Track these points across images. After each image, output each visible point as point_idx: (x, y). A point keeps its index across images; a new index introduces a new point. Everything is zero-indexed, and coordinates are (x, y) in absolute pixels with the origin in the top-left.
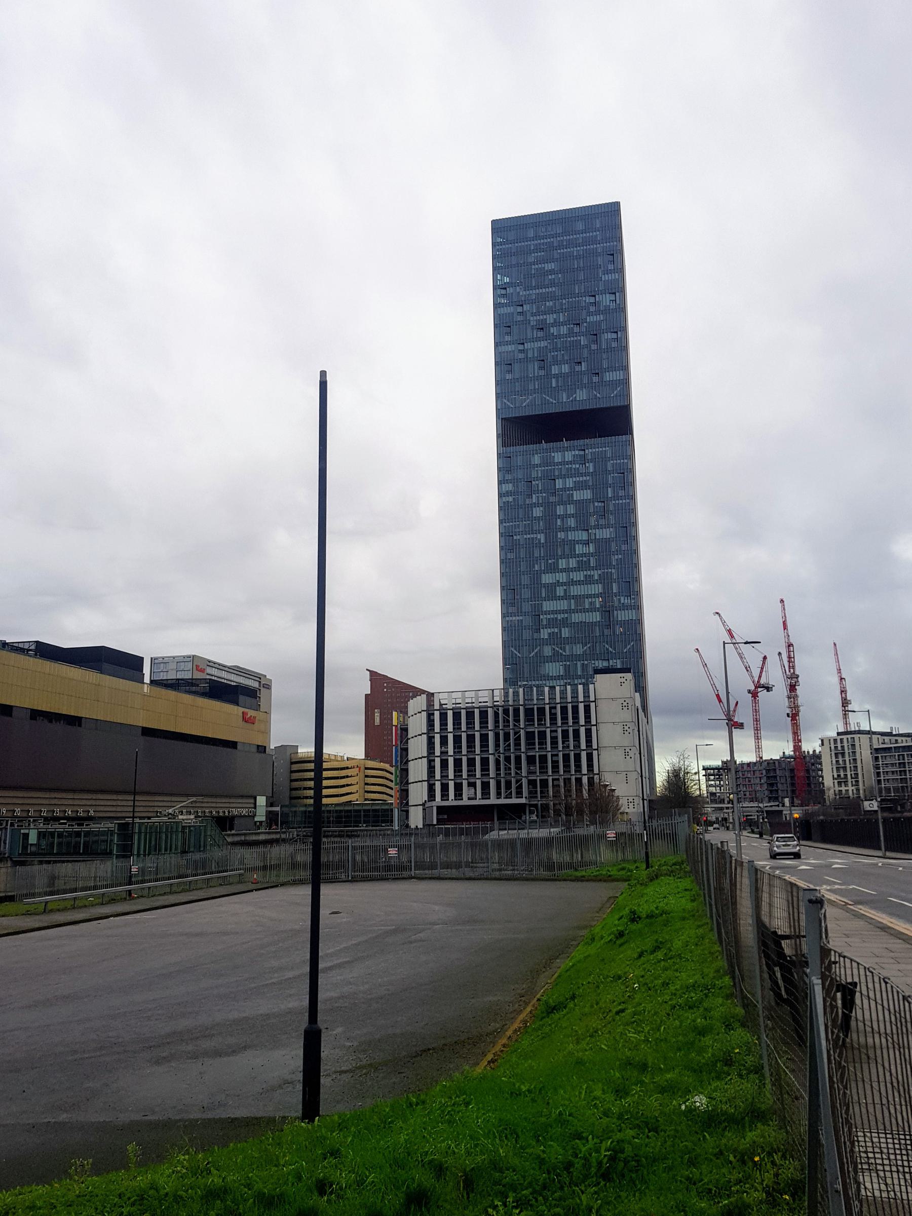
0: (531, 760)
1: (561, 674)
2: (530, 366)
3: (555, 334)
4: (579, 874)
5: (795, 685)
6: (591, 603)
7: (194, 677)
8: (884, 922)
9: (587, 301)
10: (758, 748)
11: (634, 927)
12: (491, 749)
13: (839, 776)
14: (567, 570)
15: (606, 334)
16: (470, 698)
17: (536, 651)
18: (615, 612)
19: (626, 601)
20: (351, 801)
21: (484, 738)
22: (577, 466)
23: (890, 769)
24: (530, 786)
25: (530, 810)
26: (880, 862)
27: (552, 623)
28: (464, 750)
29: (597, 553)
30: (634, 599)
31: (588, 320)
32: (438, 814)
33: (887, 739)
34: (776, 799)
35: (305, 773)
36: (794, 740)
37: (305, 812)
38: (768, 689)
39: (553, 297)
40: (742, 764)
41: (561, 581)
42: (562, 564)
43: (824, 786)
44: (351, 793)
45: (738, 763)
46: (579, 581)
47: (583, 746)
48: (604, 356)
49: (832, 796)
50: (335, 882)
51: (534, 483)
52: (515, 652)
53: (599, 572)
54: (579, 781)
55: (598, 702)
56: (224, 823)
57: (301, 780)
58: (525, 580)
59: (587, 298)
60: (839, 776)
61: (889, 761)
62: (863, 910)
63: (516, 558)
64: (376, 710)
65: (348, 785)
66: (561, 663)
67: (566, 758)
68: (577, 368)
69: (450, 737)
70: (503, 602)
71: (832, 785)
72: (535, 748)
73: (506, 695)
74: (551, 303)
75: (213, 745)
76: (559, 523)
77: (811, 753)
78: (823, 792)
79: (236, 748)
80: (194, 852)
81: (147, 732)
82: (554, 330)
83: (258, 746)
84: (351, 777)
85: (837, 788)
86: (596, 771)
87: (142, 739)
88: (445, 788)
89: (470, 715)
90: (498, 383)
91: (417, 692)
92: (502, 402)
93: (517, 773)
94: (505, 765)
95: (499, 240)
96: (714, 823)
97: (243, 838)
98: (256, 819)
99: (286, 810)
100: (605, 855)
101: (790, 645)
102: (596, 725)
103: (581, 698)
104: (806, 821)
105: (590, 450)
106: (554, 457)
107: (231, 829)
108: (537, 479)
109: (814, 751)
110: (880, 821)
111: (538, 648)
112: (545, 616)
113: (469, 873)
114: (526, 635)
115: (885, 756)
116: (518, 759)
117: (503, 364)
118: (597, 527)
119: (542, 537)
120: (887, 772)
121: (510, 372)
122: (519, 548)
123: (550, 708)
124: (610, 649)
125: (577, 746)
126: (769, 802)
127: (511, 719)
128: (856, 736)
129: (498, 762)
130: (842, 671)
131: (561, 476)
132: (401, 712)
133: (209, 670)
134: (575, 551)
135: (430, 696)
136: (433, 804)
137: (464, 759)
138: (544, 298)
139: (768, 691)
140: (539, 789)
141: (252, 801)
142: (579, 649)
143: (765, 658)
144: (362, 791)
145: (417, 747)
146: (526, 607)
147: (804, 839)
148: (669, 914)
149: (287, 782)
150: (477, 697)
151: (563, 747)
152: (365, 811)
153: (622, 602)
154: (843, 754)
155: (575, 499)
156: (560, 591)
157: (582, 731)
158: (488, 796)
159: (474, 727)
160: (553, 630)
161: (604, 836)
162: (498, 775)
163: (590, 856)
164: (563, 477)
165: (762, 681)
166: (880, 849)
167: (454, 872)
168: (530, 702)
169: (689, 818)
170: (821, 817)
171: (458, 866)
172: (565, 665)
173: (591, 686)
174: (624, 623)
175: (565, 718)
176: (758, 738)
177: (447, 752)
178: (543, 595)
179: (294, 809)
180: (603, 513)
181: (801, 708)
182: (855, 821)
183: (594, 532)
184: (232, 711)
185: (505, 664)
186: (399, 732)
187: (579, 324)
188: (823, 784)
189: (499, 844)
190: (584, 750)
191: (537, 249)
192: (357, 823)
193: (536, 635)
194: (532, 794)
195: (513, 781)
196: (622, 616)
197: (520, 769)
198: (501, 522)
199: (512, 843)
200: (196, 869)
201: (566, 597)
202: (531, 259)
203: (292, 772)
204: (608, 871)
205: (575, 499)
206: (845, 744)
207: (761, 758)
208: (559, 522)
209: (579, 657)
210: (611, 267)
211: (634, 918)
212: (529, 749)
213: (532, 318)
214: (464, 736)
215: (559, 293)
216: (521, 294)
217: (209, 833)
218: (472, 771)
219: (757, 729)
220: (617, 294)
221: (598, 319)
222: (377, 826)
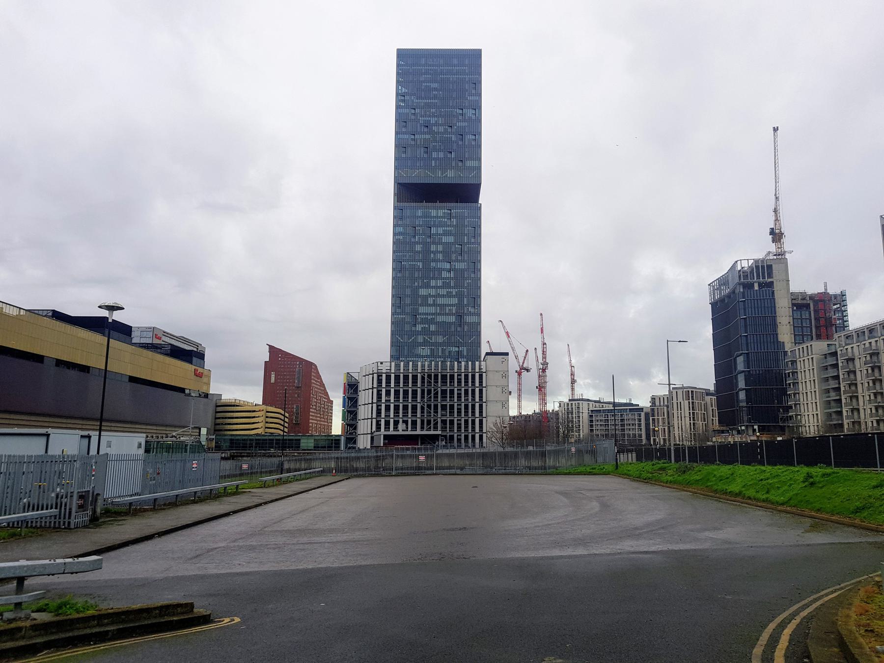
0: (444, 407)
1: (428, 354)
3: (436, 131)
7: (153, 343)
14: (437, 287)
18: (465, 317)
19: (472, 310)
23: (599, 423)
29: (455, 278)
33: (597, 404)
35: (227, 414)
38: (528, 370)
42: (433, 283)
58: (408, 292)
63: (403, 277)
64: (272, 373)
67: (466, 407)
69: (392, 391)
72: (446, 400)
73: (397, 366)
77: (551, 411)
81: (132, 379)
87: (129, 386)
88: (387, 423)
90: (396, 159)
103: (477, 370)
108: (420, 226)
110: (435, 469)
112: (420, 316)
114: (407, 327)
116: (436, 407)
117: (401, 147)
118: (457, 261)
119: (420, 265)
120: (630, 424)
124: (460, 340)
129: (422, 408)
131: (434, 226)
133: (164, 338)
138: (428, 106)
141: (198, 431)
142: (440, 339)
143: (527, 351)
146: (408, 309)
152: (277, 440)
153: (470, 310)
154: (572, 414)
156: (430, 301)
165: (525, 366)
174: (469, 324)
176: (519, 400)
183: (454, 264)
184: (188, 368)
185: (392, 346)
193: (413, 329)
197: (437, 412)
201: (434, 305)
203: (217, 412)
206: (574, 407)
209: (440, 344)
210: (473, 92)
212: (443, 400)
213: (421, 119)
216: (414, 101)
219: (519, 396)
220: (477, 110)
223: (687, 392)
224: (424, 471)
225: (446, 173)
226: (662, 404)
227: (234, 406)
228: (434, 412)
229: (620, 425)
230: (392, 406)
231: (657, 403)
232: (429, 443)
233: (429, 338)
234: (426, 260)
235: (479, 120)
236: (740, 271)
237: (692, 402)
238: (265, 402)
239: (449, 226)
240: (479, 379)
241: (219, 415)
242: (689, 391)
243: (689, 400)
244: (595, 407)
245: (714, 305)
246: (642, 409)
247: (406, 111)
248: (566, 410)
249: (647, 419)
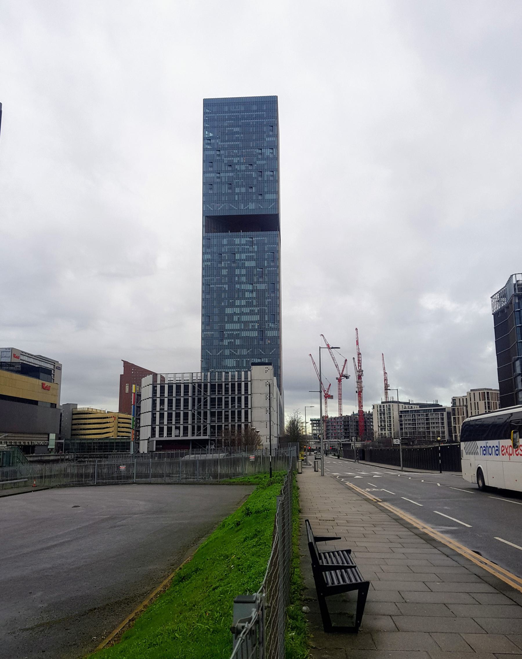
0: (213, 414)
1: (234, 365)
2: (223, 187)
3: (238, 169)
4: (232, 481)
5: (361, 376)
6: (252, 326)
8: (398, 514)
9: (257, 152)
10: (340, 410)
11: (248, 518)
12: (190, 407)
13: (381, 425)
14: (240, 306)
15: (267, 172)
16: (178, 377)
17: (220, 352)
18: (266, 332)
20: (109, 437)
21: (186, 401)
22: (248, 247)
23: (408, 422)
24: (212, 429)
25: (211, 443)
26: (399, 473)
27: (230, 337)
28: (174, 408)
29: (257, 298)
30: (276, 324)
31: (257, 163)
32: (156, 445)
33: (407, 406)
34: (348, 437)
36: (359, 405)
37: (80, 443)
38: (347, 377)
39: (238, 148)
40: (331, 418)
41: (236, 312)
42: (237, 303)
43: (373, 431)
44: (109, 432)
45: (329, 417)
46: (247, 313)
47: (243, 406)
48: (266, 185)
49: (377, 436)
50: (85, 486)
51: (223, 255)
52: (208, 352)
53: (258, 308)
54: (239, 426)
55: (253, 381)
56: (28, 449)
57: (79, 424)
58: (216, 311)
59: (257, 150)
60: (381, 425)
61: (407, 418)
62: (386, 505)
63: (211, 298)
64: (127, 384)
65: (107, 428)
66: (234, 360)
67: (233, 413)
68: (250, 190)
69: (166, 400)
70: (203, 323)
71: (377, 430)
72: (215, 407)
73: (206, 376)
74: (236, 151)
75: (22, 402)
76: (236, 279)
77: (368, 412)
78: (373, 434)
79: (37, 405)
80: (5, 466)
82: (237, 167)
83: (51, 404)
84: (109, 423)
85: (380, 432)
86: (249, 421)
88: (161, 430)
89: (178, 387)
90: (204, 195)
91: (148, 372)
92: (206, 206)
93: (204, 422)
94: (198, 417)
95: (207, 111)
96: (315, 450)
97: (40, 458)
98: (49, 447)
99: (68, 442)
100: (249, 469)
101: (359, 354)
102: (251, 395)
103: (243, 379)
104: (362, 450)
105: (256, 238)
106: (235, 241)
107: (33, 453)
108: (225, 253)
109: (369, 412)
110: (401, 450)
111: (222, 350)
112: (226, 332)
113: (167, 480)
115: (406, 415)
116: (205, 413)
117: (208, 184)
118: (258, 282)
120: (434, 423)
121: (211, 189)
122: (213, 292)
123: (225, 384)
125: (240, 406)
126: (345, 439)
127: (202, 390)
128: (391, 404)
129: (193, 415)
130: (386, 369)
132: (138, 385)
133: (22, 357)
134: (245, 296)
135: (155, 375)
136: (154, 439)
137: (174, 413)
138: (232, 147)
139: (347, 378)
140: (216, 431)
141: (47, 436)
142: (245, 352)
143: (346, 360)
144: (116, 432)
145: (146, 406)
146: (216, 327)
147: (361, 460)
148: (268, 510)
149: (70, 426)
150: (183, 377)
151: (231, 407)
152: (116, 443)
153: (270, 326)
154: (384, 414)
155: (246, 266)
156: (236, 318)
157: (243, 398)
158: (187, 435)
159: (180, 395)
160: (230, 340)
161: (249, 458)
162: (193, 422)
163: (239, 470)
164: (240, 253)
165: (344, 373)
166: (400, 466)
167: (159, 480)
168: (214, 381)
169: (297, 449)
170: (371, 448)
171: (162, 476)
172: (237, 360)
173: (249, 372)
175: (233, 390)
176: (340, 404)
177: (164, 409)
178: (226, 320)
179: (73, 441)
180: (262, 275)
181: (363, 388)
182: (388, 450)
186: (136, 396)
187: (252, 165)
188: (373, 429)
189: (187, 463)
190: (243, 409)
191: (230, 119)
192: (111, 450)
193: (221, 343)
194: (213, 434)
195: (202, 426)
196: (270, 334)
197: (206, 419)
198: (203, 276)
199: (194, 462)
200: (7, 477)
201: (239, 322)
202: (226, 124)
203: (73, 419)
204: (249, 479)
205: (246, 266)
206: (385, 408)
207: (342, 415)
208: (236, 279)
209: (244, 357)
210: (271, 133)
211: (248, 513)
212: (212, 408)
214: (174, 399)
215: (241, 146)
216: (219, 144)
217: (16, 455)
218: (178, 420)
219: (340, 399)
221: (263, 163)
222: (124, 451)
223: (483, 393)
224: (125, 480)
225: (248, 206)
226: (462, 404)
227: (87, 413)
228: (204, 419)
229: (425, 424)
230: (166, 414)
231: (458, 404)
232: (200, 448)
233: (235, 351)
234: (231, 282)
235: (276, 158)
236: (515, 284)
237: (488, 402)
238: (121, 410)
239: (251, 252)
240: (245, 388)
241: (75, 422)
242: (484, 392)
243: (485, 400)
244: (405, 408)
245: (495, 315)
246: (444, 410)
247: (212, 153)
248: (379, 410)
249: (449, 418)
